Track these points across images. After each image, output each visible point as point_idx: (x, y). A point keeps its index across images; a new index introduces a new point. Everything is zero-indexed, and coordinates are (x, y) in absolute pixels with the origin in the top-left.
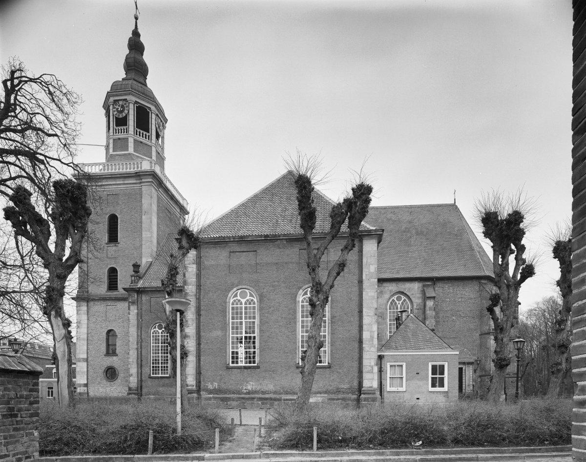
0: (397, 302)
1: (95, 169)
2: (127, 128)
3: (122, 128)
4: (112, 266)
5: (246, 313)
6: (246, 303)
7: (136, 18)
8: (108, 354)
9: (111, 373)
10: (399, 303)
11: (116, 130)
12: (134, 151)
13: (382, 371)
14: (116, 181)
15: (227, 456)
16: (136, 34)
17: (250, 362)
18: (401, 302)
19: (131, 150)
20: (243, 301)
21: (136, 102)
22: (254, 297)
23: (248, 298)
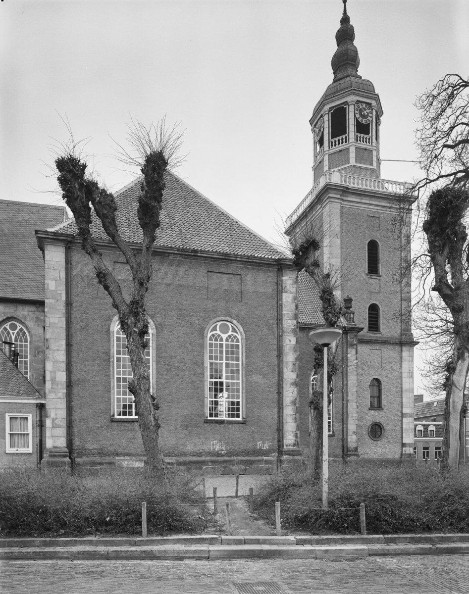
0: (11, 332)
2: (346, 137)
3: (362, 135)
4: (375, 302)
5: (221, 352)
6: (227, 340)
8: (372, 407)
9: (376, 431)
10: (13, 333)
11: (332, 143)
13: (38, 426)
14: (362, 199)
15: (237, 540)
16: (345, 20)
17: (233, 416)
18: (16, 332)
20: (224, 336)
22: (237, 333)
23: (230, 333)
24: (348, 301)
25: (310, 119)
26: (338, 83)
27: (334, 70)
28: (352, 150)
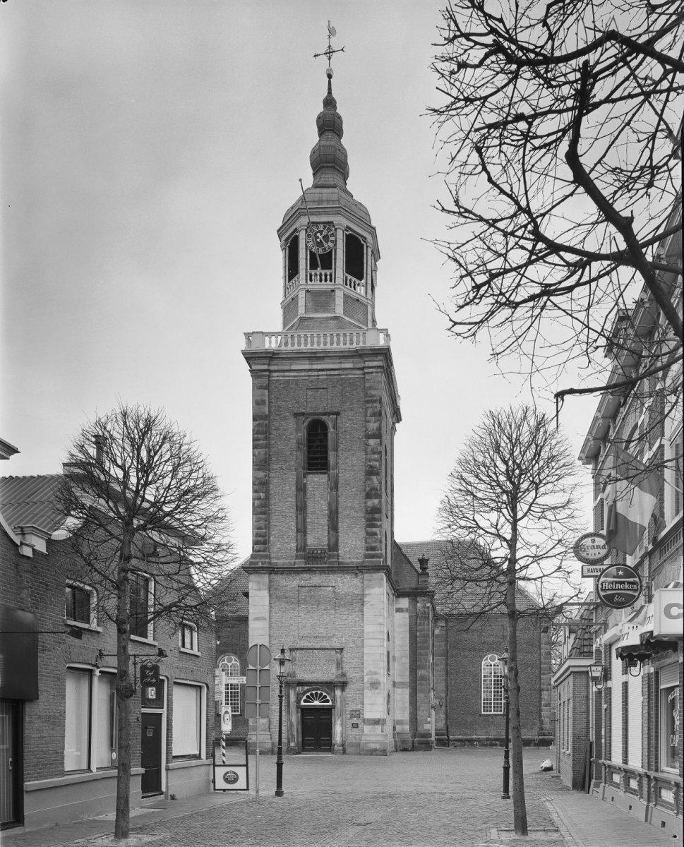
1: (270, 343)
3: (354, 279)
6: (231, 666)
7: (330, 76)
12: (345, 314)
16: (329, 102)
19: (339, 310)
21: (348, 228)
23: (233, 662)
24: (617, 658)
25: (278, 228)
26: (318, 190)
27: (313, 169)
28: (339, 296)
